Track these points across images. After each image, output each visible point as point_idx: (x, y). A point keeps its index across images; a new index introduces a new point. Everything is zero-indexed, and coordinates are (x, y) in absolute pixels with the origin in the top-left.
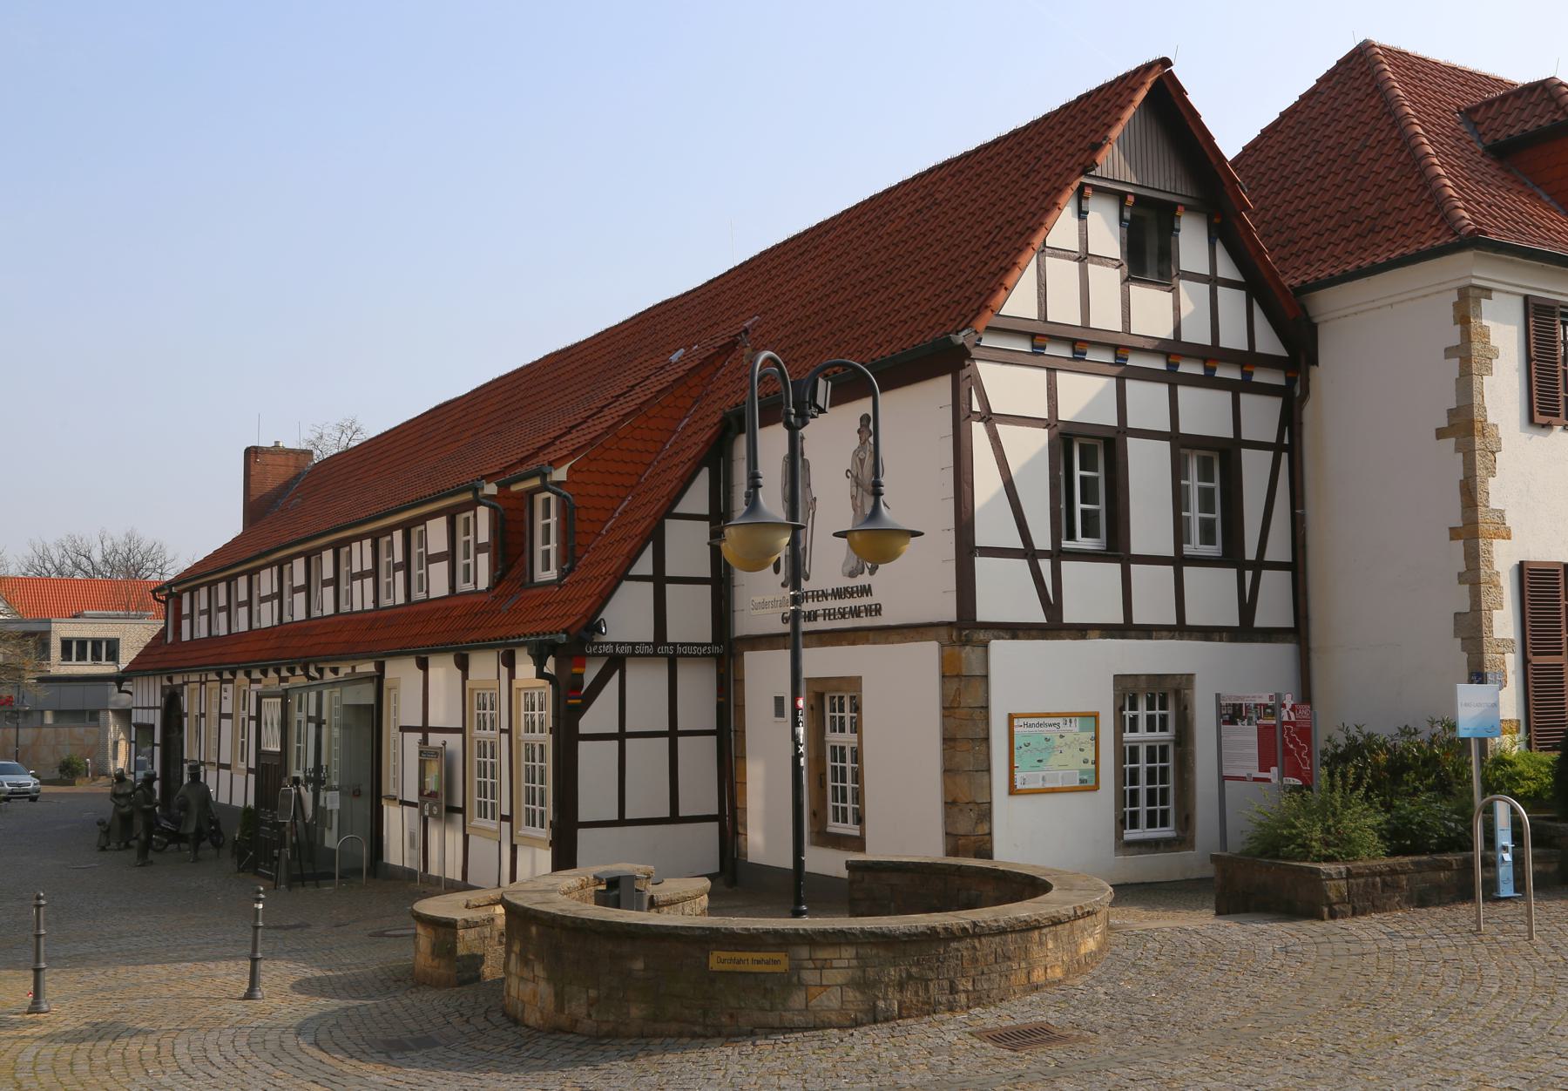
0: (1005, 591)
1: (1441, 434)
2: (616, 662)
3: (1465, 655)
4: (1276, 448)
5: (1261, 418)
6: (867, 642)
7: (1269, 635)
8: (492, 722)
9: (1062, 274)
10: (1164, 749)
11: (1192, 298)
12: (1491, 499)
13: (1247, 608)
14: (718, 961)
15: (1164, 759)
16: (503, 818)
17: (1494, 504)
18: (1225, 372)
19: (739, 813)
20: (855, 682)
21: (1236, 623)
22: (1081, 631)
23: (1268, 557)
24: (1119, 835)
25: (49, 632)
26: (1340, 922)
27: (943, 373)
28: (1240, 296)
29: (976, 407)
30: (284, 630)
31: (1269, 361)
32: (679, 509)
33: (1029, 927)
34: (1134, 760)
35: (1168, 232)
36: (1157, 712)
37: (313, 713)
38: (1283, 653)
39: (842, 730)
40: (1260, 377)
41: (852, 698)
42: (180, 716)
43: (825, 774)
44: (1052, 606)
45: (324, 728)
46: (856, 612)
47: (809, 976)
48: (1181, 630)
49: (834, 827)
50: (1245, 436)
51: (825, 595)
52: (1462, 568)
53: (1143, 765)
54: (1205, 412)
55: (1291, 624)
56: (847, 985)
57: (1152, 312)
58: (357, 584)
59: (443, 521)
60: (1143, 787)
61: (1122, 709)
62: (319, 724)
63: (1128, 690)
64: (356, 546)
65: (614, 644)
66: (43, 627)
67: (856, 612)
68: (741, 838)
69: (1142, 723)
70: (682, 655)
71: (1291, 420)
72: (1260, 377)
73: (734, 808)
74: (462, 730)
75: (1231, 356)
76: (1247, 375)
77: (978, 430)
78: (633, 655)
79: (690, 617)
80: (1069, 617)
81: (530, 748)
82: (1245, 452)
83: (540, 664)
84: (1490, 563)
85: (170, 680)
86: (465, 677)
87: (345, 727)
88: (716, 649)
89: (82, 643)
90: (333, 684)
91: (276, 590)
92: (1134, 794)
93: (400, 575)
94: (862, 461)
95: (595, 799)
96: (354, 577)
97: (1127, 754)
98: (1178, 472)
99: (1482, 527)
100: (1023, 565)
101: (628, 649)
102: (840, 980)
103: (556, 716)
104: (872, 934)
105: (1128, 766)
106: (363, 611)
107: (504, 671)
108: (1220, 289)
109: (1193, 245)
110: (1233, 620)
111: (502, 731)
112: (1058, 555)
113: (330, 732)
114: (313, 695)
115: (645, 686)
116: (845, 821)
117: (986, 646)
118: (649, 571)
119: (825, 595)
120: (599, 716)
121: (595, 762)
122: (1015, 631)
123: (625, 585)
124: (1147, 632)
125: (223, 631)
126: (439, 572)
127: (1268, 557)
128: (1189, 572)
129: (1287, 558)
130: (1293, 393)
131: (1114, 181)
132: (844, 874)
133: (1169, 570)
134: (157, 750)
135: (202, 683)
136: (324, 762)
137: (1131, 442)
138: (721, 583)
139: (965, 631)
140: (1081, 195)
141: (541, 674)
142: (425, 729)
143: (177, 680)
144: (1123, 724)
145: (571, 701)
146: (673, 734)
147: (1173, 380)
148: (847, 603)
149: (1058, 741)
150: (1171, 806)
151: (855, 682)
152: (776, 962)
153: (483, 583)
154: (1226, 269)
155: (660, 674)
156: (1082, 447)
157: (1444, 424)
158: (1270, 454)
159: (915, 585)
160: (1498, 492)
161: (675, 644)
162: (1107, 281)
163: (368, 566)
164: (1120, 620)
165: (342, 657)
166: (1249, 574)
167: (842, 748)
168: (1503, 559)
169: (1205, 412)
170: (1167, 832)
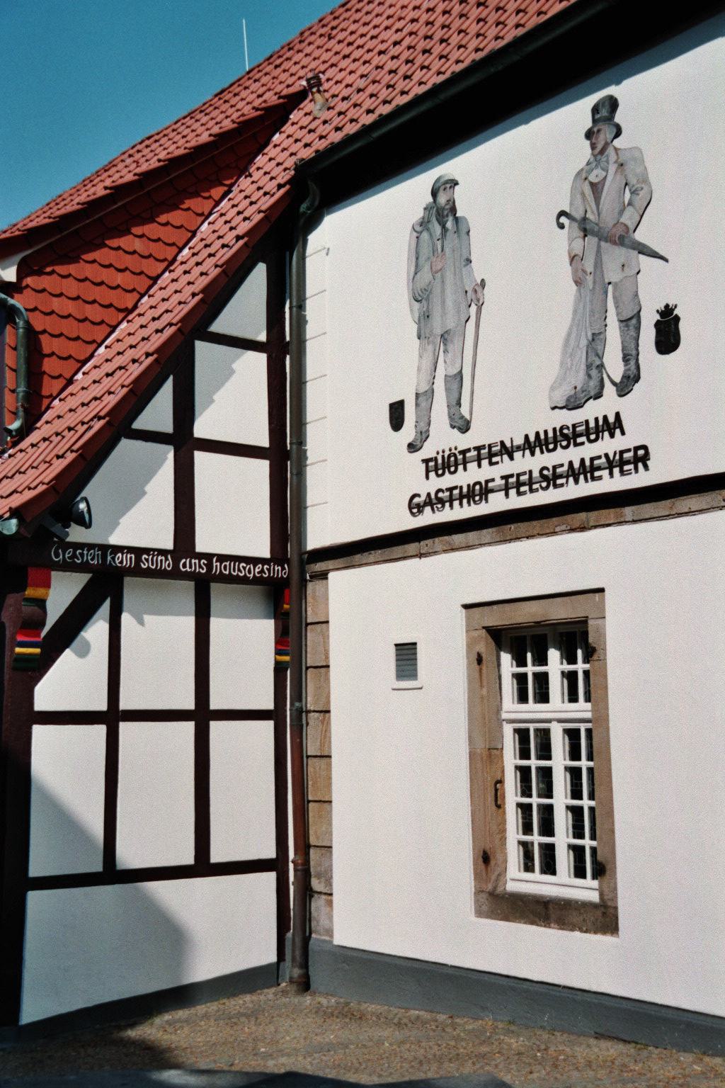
2: (109, 581)
32: (217, 327)
46: (587, 470)
51: (508, 451)
67: (587, 470)
69: (556, 686)
73: (304, 847)
78: (137, 571)
79: (234, 516)
88: (278, 571)
94: (596, 188)
115: (156, 640)
118: (167, 426)
119: (508, 451)
123: (125, 444)
138: (284, 455)
161: (209, 557)
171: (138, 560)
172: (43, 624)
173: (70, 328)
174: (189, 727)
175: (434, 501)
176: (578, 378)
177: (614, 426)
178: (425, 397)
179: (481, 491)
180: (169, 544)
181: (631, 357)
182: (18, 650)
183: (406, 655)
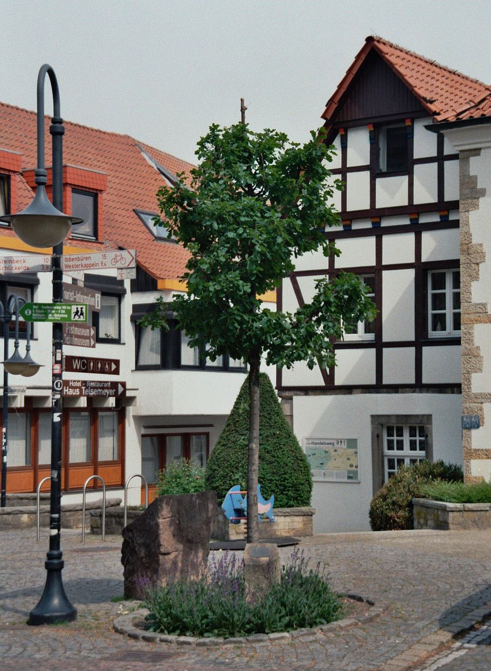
22: (348, 389)
36: (395, 438)
44: (329, 378)
48: (419, 386)
50: (412, 260)
57: (392, 192)
69: (407, 445)
80: (338, 382)
117: (291, 399)
124: (395, 388)
131: (383, 116)
147: (417, 229)
149: (334, 453)
156: (433, 275)
168: (11, 174)
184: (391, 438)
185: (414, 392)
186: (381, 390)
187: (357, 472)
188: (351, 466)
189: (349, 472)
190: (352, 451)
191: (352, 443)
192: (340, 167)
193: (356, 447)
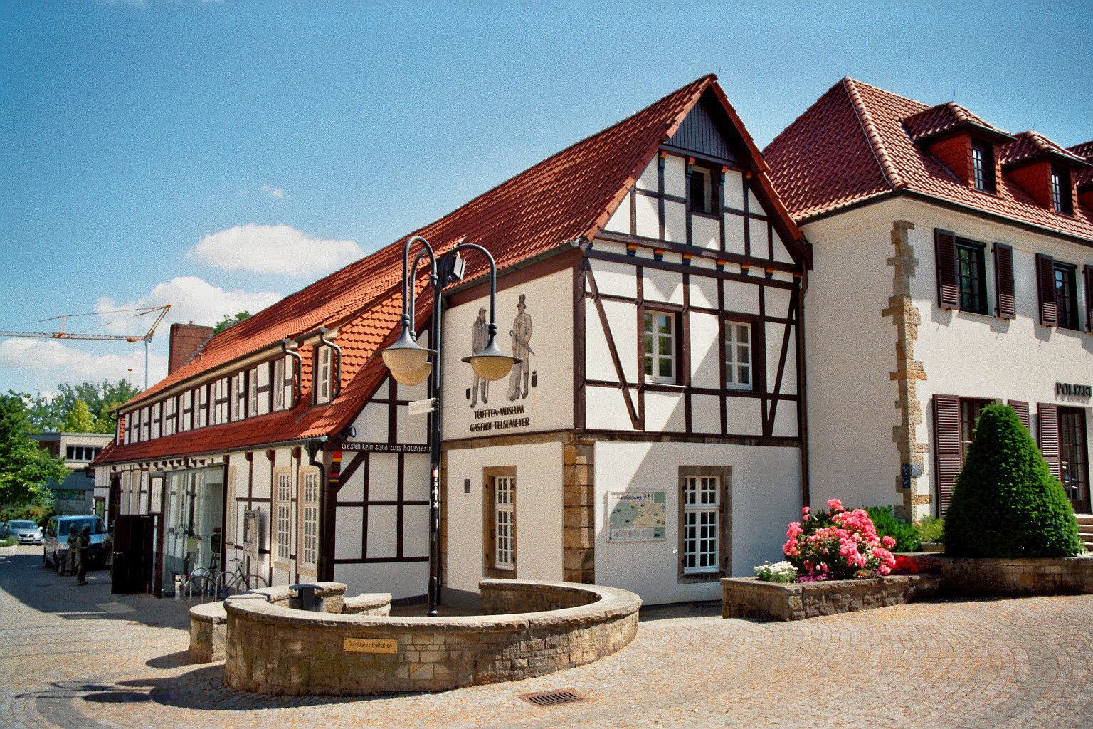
0: (606, 409)
1: (885, 313)
2: (363, 455)
3: (899, 453)
4: (788, 322)
5: (778, 303)
6: (520, 442)
7: (782, 441)
8: (288, 494)
9: (646, 207)
10: (712, 515)
11: (734, 223)
12: (914, 354)
13: (768, 424)
14: (350, 645)
15: (712, 521)
16: (292, 557)
17: (916, 357)
18: (756, 272)
19: (443, 556)
20: (512, 470)
21: (761, 434)
23: (782, 392)
24: (681, 571)
25: (59, 441)
26: (796, 623)
27: (569, 267)
28: (763, 226)
29: (588, 289)
30: (179, 437)
31: (783, 267)
33: (568, 627)
34: (693, 521)
35: (718, 181)
37: (189, 490)
38: (791, 453)
39: (505, 501)
40: (779, 276)
41: (511, 480)
42: (120, 491)
43: (494, 530)
44: (638, 421)
45: (196, 499)
46: (514, 424)
47: (413, 657)
48: (724, 437)
49: (500, 565)
51: (496, 413)
52: (897, 398)
53: (698, 526)
54: (742, 298)
55: (795, 434)
56: (438, 662)
57: (706, 234)
58: (219, 406)
59: (266, 365)
60: (698, 539)
61: (685, 488)
62: (193, 497)
63: (687, 476)
64: (219, 382)
65: (361, 444)
66: (56, 438)
67: (514, 424)
68: (444, 572)
70: (407, 452)
71: (797, 304)
72: (779, 276)
74: (270, 500)
75: (758, 262)
76: (769, 275)
77: (590, 304)
78: (374, 451)
81: (308, 512)
82: (767, 324)
83: (312, 456)
84: (914, 395)
85: (114, 469)
86: (273, 465)
87: (207, 498)
89: (80, 449)
90: (201, 468)
91: (175, 412)
92: (692, 544)
93: (242, 400)
94: (519, 325)
95: (346, 545)
96: (217, 402)
97: (687, 519)
98: (723, 335)
99: (909, 372)
100: (618, 393)
101: (370, 447)
102: (432, 660)
103: (322, 490)
104: (456, 628)
105: (688, 526)
106: (222, 424)
107: (295, 460)
108: (751, 221)
109: (733, 189)
110: (759, 432)
111: (292, 500)
112: (643, 388)
113: (199, 502)
114: (190, 475)
115: (383, 468)
116: (506, 561)
117: (592, 445)
120: (351, 490)
121: (347, 520)
122: (612, 436)
123: (370, 405)
124: (702, 438)
125: (146, 439)
126: (264, 398)
127: (782, 392)
128: (729, 399)
129: (794, 392)
130: (799, 288)
132: (478, 591)
133: (717, 398)
134: (107, 513)
135: (131, 471)
136: (195, 521)
137: (692, 314)
139: (580, 437)
140: (660, 153)
141: (313, 463)
142: (250, 499)
143: (119, 469)
144: (686, 498)
145: (332, 481)
146: (400, 503)
147: (720, 276)
148: (509, 418)
149: (640, 509)
150: (717, 553)
151: (512, 470)
152: (388, 646)
153: (288, 405)
154: (755, 207)
155: (392, 461)
157: (886, 306)
158: (784, 326)
159: (548, 406)
160: (919, 351)
161: (402, 445)
162: (676, 212)
163: (225, 395)
164: (684, 430)
165: (202, 453)
166: (769, 402)
167: (506, 514)
168: (921, 394)
169: (742, 298)
170: (709, 569)
171: (374, 447)
172: (339, 471)
173: (351, 353)
174: (395, 508)
175: (477, 428)
176: (513, 391)
177: (520, 409)
178: (476, 388)
179: (488, 426)
180: (386, 441)
181: (526, 387)
182: (331, 480)
183: (467, 483)
184: (712, 491)
185: (718, 442)
186: (690, 439)
187: (664, 529)
188: (658, 522)
189: (656, 529)
190: (658, 505)
191: (660, 497)
192: (743, 217)
193: (664, 501)
